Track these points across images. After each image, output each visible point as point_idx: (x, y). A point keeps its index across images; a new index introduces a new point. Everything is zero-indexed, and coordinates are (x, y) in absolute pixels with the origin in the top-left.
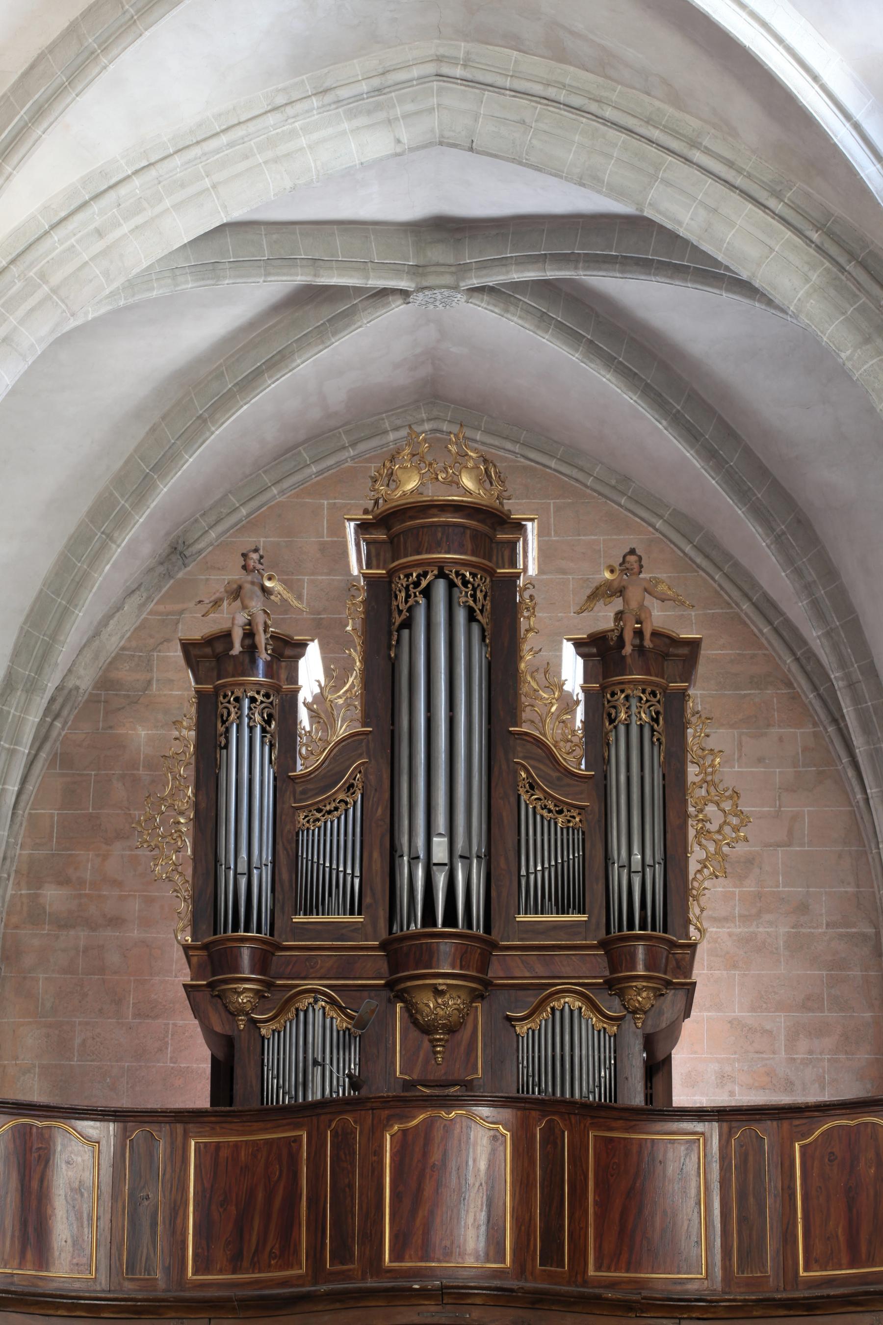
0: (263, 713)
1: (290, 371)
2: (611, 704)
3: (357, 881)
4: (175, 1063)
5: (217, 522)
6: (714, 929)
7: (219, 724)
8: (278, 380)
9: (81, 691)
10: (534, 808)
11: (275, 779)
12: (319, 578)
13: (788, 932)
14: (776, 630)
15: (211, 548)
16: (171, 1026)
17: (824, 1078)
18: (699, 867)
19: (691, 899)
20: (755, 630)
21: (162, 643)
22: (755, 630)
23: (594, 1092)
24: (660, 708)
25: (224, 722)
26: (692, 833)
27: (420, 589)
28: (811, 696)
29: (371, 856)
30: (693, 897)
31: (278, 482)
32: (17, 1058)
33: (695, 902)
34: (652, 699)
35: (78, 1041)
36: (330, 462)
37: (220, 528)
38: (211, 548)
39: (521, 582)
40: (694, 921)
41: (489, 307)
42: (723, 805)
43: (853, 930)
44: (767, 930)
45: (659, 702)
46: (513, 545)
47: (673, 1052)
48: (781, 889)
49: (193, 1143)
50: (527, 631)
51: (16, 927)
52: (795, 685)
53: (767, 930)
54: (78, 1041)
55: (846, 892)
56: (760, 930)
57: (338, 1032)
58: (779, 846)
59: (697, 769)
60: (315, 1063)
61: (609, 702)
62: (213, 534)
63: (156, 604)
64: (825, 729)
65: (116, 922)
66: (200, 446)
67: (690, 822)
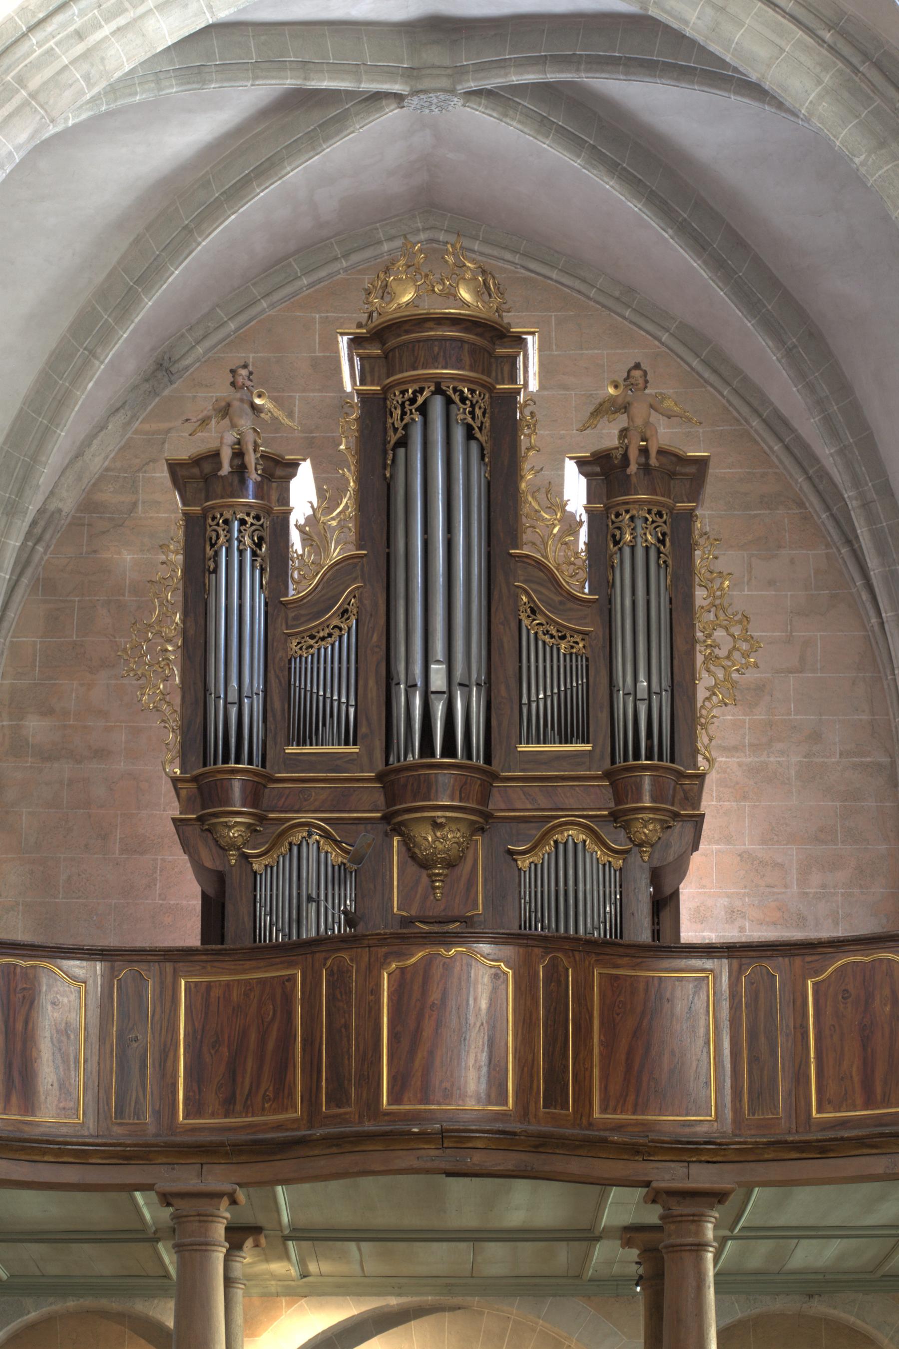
0: (253, 536)
1: (280, 178)
2: (615, 525)
3: (352, 710)
4: (164, 900)
5: (205, 337)
6: (724, 759)
7: (208, 547)
8: (267, 188)
9: (64, 514)
10: (536, 633)
11: (266, 604)
13: (800, 762)
14: (787, 448)
15: (197, 365)
18: (708, 694)
19: (699, 727)
20: (766, 448)
21: (147, 464)
22: (766, 448)
23: (599, 928)
24: (666, 529)
26: (700, 659)
28: (824, 516)
30: (701, 725)
31: (268, 295)
33: (704, 731)
37: (208, 343)
38: (197, 365)
39: (521, 398)
41: (487, 112)
43: (868, 759)
44: (778, 759)
45: (665, 522)
46: (513, 359)
47: (681, 886)
48: (792, 717)
49: (183, 982)
52: (807, 505)
53: (778, 759)
55: (861, 720)
56: (771, 759)
57: (333, 866)
58: (791, 672)
60: (310, 899)
61: (613, 522)
62: (200, 350)
63: (141, 422)
64: (839, 551)
65: (101, 753)
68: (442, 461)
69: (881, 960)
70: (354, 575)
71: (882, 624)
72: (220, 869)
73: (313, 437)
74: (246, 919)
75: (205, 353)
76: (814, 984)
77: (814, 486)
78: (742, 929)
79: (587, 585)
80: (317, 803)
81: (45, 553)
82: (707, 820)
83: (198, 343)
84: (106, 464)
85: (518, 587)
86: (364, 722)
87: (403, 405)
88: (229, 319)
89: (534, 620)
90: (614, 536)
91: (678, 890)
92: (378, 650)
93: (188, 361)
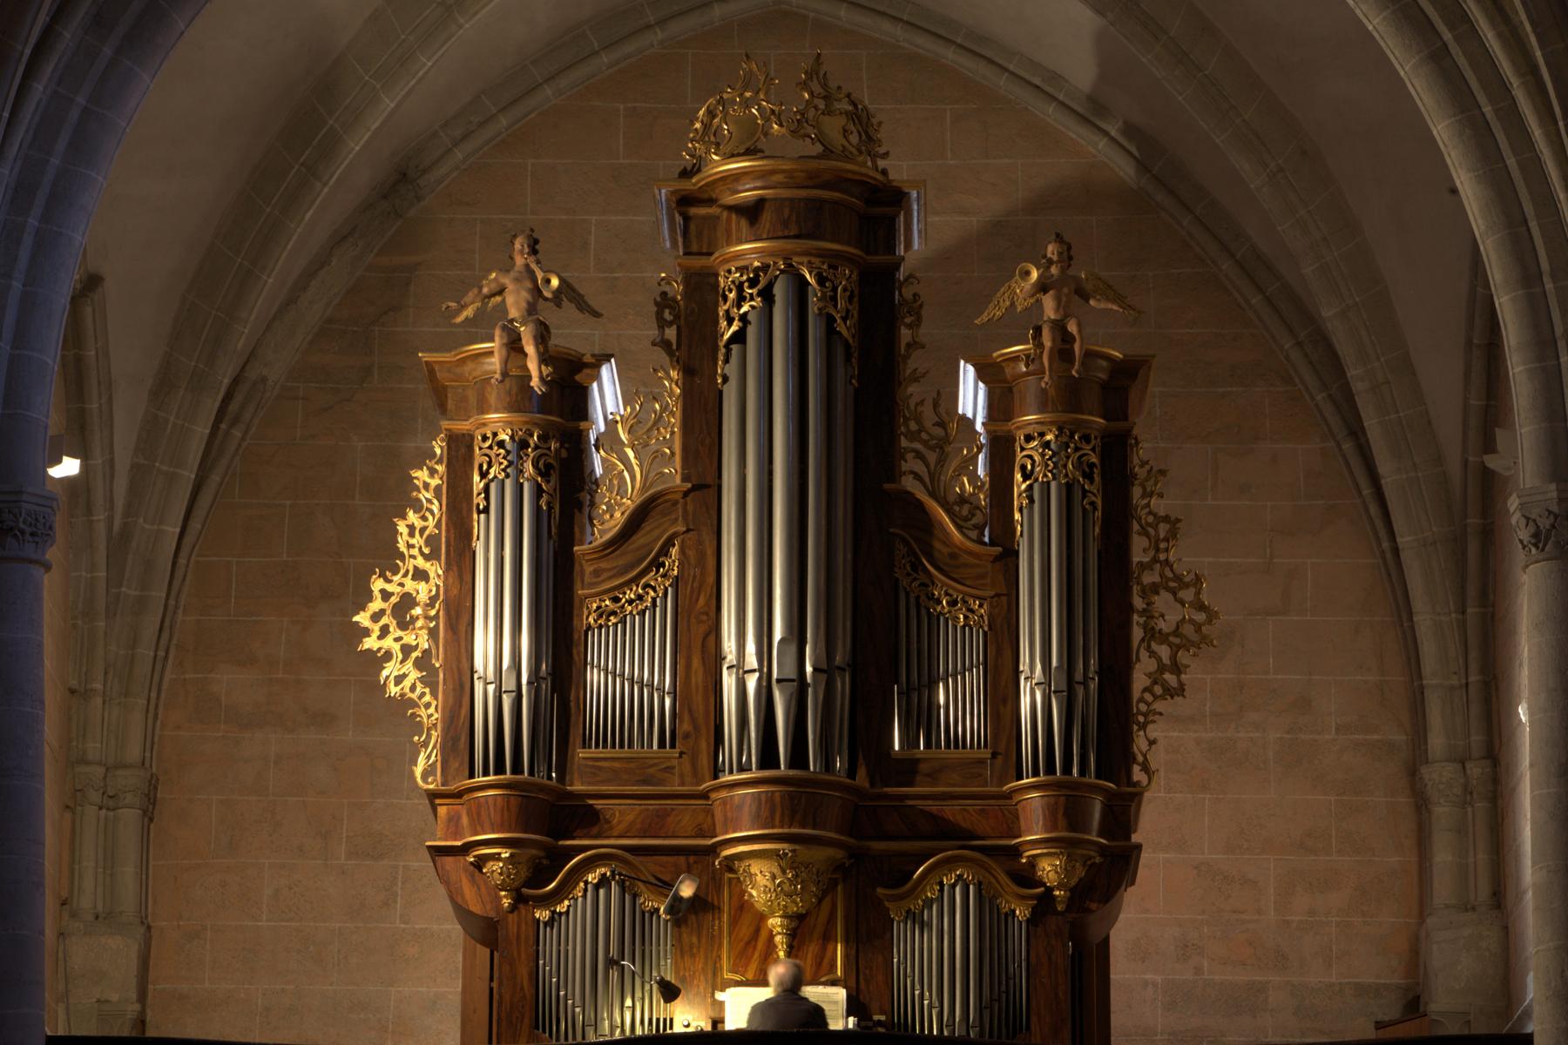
7: (476, 478)
10: (918, 597)
11: (555, 553)
15: (455, 174)
18: (1148, 682)
23: (999, 1000)
24: (1094, 459)
26: (1137, 633)
27: (760, 286)
29: (688, 666)
30: (1138, 724)
34: (1084, 445)
38: (455, 174)
39: (901, 275)
43: (1375, 737)
45: (1093, 450)
46: (892, 221)
47: (1112, 933)
52: (1297, 380)
57: (643, 913)
59: (1144, 542)
61: (1023, 449)
62: (459, 155)
64: (1339, 445)
67: (1135, 617)
68: (787, 417)
78: (1198, 970)
79: (987, 533)
80: (622, 827)
82: (1145, 856)
83: (456, 145)
86: (686, 717)
90: (1023, 468)
92: (704, 618)
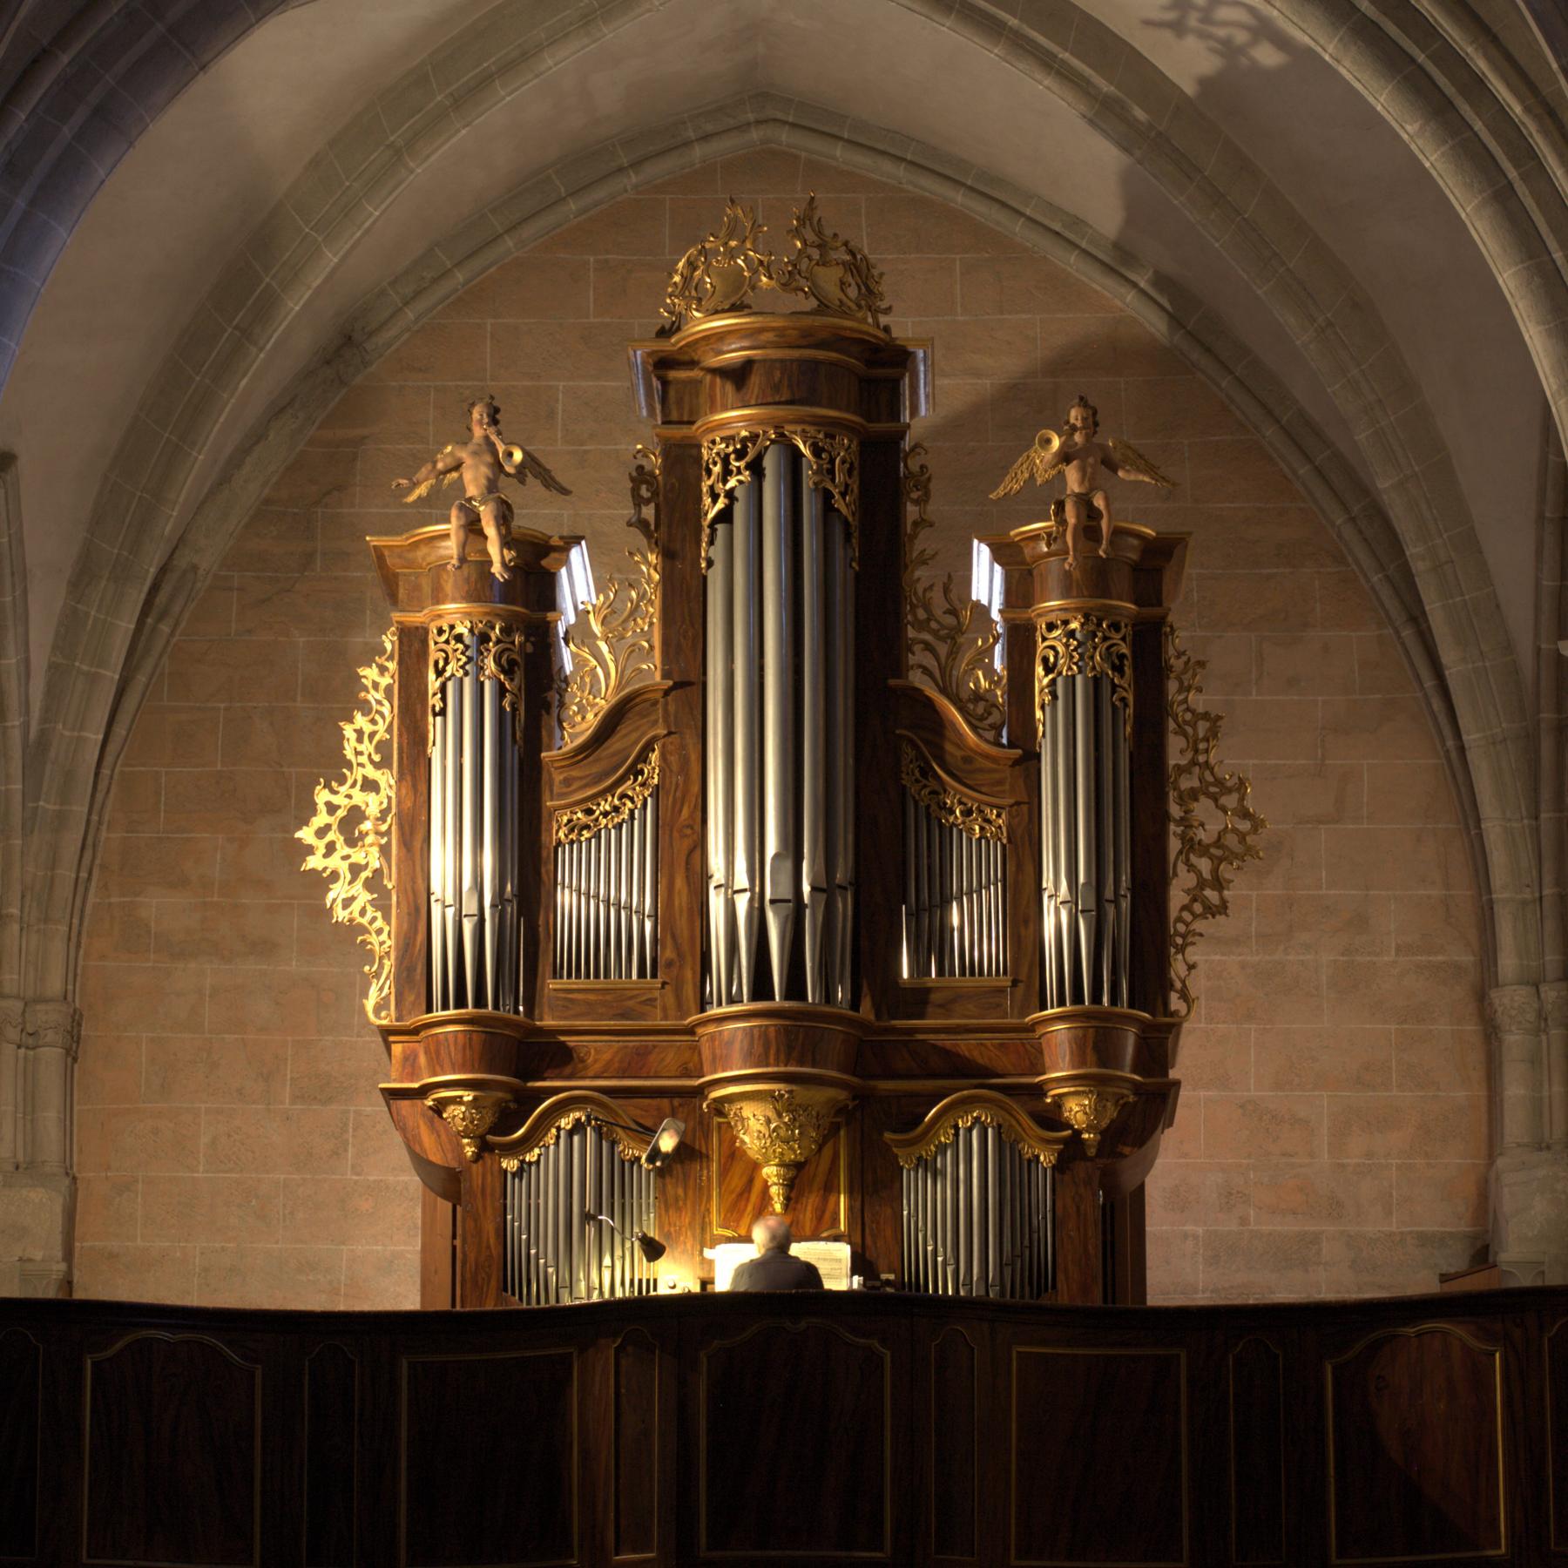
2: (1047, 643)
3: (648, 925)
5: (417, 294)
6: (1218, 957)
9: (201, 572)
11: (521, 763)
12: (584, 384)
13: (1335, 961)
14: (1318, 471)
15: (406, 336)
16: (352, 1116)
17: (1391, 1195)
18: (1186, 899)
19: (1173, 950)
20: (1286, 470)
21: (329, 493)
22: (1286, 470)
24: (1125, 650)
25: (439, 673)
26: (1174, 845)
31: (514, 228)
32: (109, 1168)
33: (1180, 957)
35: (205, 1140)
36: (599, 193)
38: (406, 336)
39: (907, 444)
40: (1178, 985)
42: (1223, 800)
43: (1440, 958)
45: (1123, 639)
46: (895, 385)
47: (1148, 1180)
48: (1324, 892)
50: (915, 524)
51: (103, 957)
52: (1350, 559)
54: (205, 1140)
55: (1429, 897)
56: (1290, 958)
57: (623, 1162)
58: (1320, 822)
60: (587, 1217)
61: (1044, 639)
62: (410, 315)
63: (319, 428)
64: (1397, 632)
65: (264, 948)
66: (390, 193)
67: (1172, 827)
69: (1432, 1332)
70: (653, 718)
71: (1462, 749)
72: (454, 1164)
73: (586, 452)
74: (492, 1241)
75: (417, 319)
76: (1334, 1368)
77: (1360, 532)
78: (1244, 1221)
80: (597, 1066)
81: (172, 634)
82: (1184, 1094)
83: (406, 304)
84: (266, 491)
85: (901, 737)
87: (726, 461)
88: (456, 265)
89: (925, 786)
91: (1142, 1187)
92: (689, 831)
93: (387, 335)
